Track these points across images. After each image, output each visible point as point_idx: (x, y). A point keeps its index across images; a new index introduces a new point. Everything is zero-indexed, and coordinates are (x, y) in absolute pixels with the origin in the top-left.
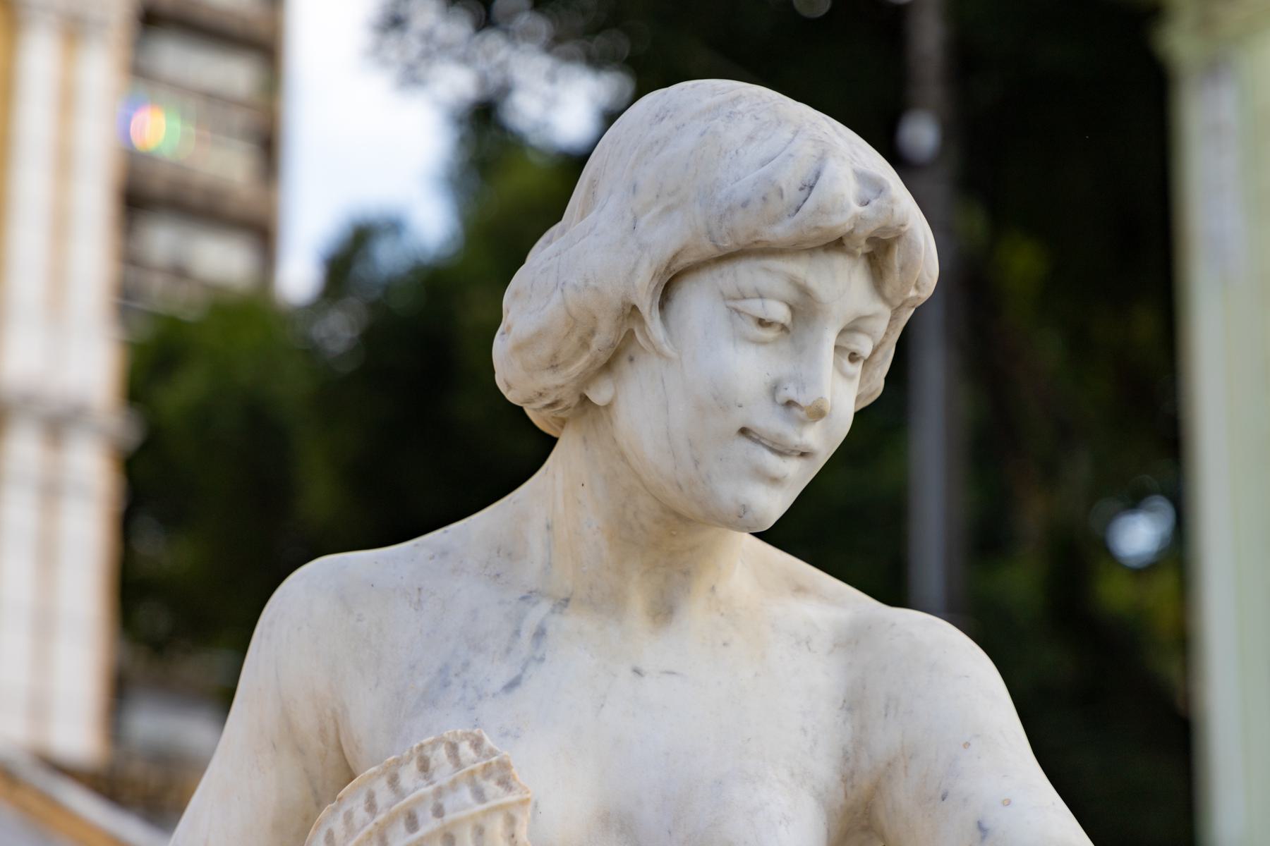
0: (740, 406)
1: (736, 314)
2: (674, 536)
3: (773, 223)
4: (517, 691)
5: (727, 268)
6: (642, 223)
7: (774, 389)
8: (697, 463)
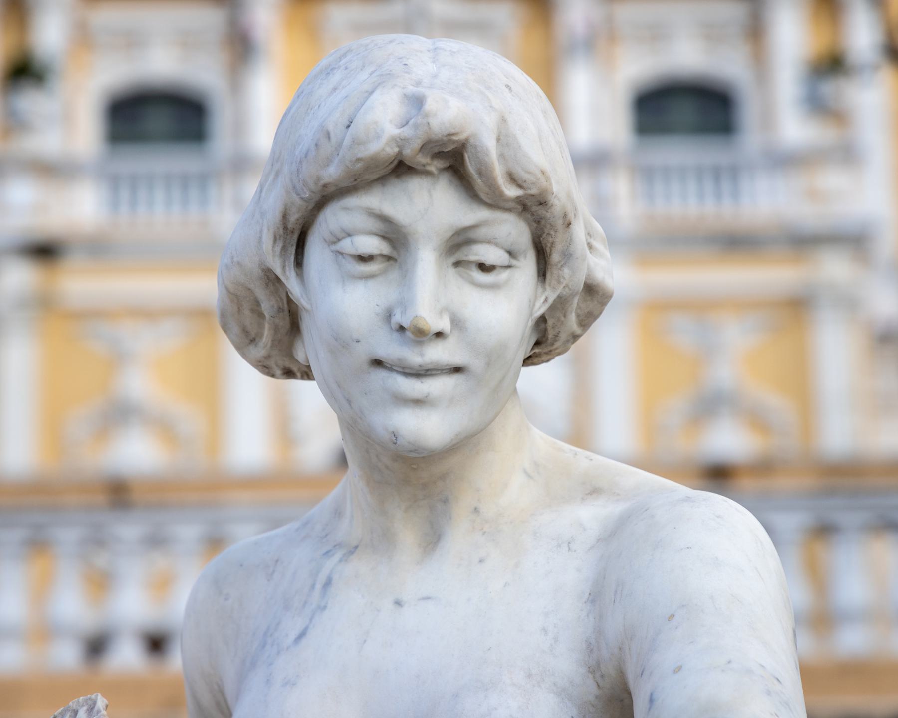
0: (358, 341)
1: (340, 257)
2: (414, 469)
3: (328, 165)
4: (304, 641)
7: (388, 315)
8: (349, 402)
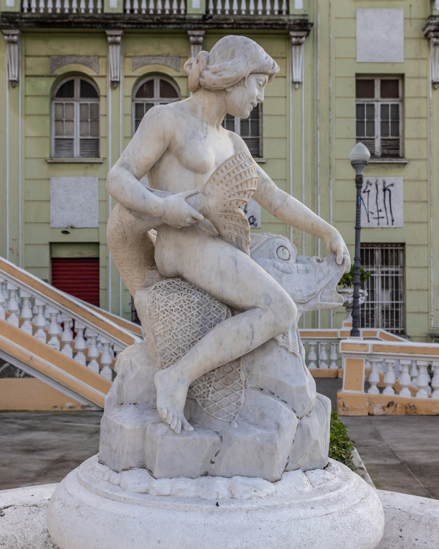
5: (259, 75)
6: (249, 63)
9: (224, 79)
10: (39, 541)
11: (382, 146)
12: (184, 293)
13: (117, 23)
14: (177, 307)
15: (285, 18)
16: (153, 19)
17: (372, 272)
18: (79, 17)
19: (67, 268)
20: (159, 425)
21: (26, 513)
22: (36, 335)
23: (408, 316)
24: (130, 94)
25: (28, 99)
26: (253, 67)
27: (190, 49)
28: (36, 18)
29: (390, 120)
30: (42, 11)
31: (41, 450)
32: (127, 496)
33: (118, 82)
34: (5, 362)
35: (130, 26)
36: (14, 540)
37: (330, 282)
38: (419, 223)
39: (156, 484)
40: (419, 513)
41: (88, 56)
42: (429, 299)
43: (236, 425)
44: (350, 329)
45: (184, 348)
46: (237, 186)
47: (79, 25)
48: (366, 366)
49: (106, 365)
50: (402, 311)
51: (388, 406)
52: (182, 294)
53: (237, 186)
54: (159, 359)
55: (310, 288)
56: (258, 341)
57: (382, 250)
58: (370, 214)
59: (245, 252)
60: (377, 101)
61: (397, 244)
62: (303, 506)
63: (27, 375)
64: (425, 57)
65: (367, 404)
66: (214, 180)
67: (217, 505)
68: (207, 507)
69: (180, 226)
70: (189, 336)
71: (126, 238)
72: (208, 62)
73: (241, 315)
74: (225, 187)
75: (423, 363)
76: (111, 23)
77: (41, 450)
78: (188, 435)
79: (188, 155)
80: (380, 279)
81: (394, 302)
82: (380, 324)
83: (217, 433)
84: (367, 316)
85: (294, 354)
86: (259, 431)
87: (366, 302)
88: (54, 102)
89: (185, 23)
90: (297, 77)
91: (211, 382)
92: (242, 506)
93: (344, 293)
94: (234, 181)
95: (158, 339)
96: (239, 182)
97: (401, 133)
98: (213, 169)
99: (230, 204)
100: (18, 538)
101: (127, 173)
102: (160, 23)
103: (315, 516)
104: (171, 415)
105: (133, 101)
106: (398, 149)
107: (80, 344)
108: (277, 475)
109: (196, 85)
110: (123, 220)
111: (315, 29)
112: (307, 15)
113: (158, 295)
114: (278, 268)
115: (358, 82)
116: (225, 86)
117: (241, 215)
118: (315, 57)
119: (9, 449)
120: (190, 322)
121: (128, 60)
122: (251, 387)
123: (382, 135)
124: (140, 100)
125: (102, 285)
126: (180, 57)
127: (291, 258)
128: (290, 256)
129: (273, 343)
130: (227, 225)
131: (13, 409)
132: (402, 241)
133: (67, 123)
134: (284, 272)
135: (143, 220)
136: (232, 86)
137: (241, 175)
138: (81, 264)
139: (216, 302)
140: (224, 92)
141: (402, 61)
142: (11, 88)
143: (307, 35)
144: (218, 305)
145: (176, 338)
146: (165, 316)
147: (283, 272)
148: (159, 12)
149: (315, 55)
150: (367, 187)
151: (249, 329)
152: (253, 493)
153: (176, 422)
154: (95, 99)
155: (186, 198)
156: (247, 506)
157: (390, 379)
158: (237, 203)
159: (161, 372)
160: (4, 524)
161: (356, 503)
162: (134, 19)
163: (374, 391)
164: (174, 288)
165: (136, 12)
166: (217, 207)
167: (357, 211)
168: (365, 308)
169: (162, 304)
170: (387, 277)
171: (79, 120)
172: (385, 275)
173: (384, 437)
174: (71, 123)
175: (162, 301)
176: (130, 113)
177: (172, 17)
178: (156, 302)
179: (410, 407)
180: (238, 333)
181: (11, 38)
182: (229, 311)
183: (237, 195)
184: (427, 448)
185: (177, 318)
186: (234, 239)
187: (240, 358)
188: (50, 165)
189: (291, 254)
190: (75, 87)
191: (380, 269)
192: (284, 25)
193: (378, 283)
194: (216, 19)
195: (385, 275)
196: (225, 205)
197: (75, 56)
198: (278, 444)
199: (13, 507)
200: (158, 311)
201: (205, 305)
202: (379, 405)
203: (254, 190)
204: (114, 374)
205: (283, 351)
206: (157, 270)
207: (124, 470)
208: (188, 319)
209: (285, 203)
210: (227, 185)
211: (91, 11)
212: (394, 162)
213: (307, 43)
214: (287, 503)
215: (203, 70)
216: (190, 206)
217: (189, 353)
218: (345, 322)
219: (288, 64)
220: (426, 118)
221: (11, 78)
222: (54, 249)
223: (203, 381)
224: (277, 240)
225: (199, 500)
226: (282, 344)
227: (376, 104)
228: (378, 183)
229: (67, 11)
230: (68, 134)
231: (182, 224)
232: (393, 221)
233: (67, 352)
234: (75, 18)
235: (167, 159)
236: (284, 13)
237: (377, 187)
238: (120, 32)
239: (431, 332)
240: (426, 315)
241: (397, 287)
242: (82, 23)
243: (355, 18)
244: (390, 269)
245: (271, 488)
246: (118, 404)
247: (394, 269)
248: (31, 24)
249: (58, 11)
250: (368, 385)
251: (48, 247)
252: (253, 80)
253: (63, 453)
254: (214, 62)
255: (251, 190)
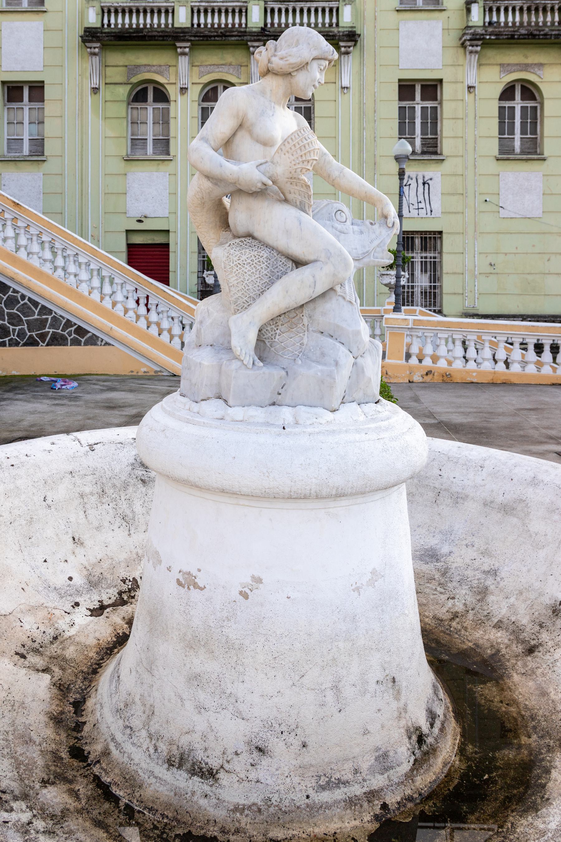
5: (320, 60)
9: (290, 64)
10: (124, 473)
11: (422, 144)
12: (254, 249)
13: (185, 36)
14: (249, 261)
15: (335, 30)
16: (217, 32)
17: (413, 258)
18: (152, 31)
19: (142, 253)
20: (233, 361)
21: (113, 449)
22: (115, 308)
23: (445, 297)
24: (197, 99)
25: (108, 104)
26: (315, 54)
27: (250, 59)
28: (115, 33)
29: (429, 121)
30: (120, 26)
31: (120, 407)
32: (206, 421)
33: (186, 89)
34: (89, 332)
35: (197, 38)
36: (103, 471)
37: (381, 242)
38: (455, 213)
39: (230, 411)
40: (457, 455)
41: (160, 66)
42: (464, 281)
43: (300, 362)
44: (392, 307)
45: (255, 297)
46: (301, 156)
47: (152, 38)
48: (407, 340)
49: (176, 335)
50: (439, 293)
51: (427, 374)
52: (253, 250)
53: (301, 156)
54: (233, 307)
55: (364, 247)
56: (320, 290)
57: (421, 238)
58: (411, 205)
59: (307, 214)
60: (418, 104)
61: (435, 233)
62: (358, 431)
63: (107, 344)
64: (461, 63)
65: (408, 372)
66: (282, 151)
67: (284, 428)
68: (275, 430)
69: (252, 191)
70: (258, 286)
71: (204, 203)
72: (275, 50)
73: (304, 267)
74: (291, 156)
75: (458, 337)
76: (180, 36)
77: (120, 407)
78: (258, 369)
79: (258, 130)
80: (420, 264)
81: (432, 284)
82: (419, 304)
83: (284, 368)
84: (408, 296)
85: (350, 302)
86: (320, 367)
87: (406, 284)
88: (130, 106)
89: (246, 36)
90: (346, 82)
91: (278, 326)
92: (305, 430)
93: (387, 275)
94: (299, 151)
95: (232, 289)
96: (303, 153)
97: (439, 132)
98: (279, 142)
99: (295, 172)
100: (106, 469)
101: (205, 145)
102: (223, 35)
103: (369, 440)
104: (244, 353)
105: (199, 105)
106: (436, 147)
107: (153, 316)
108: (335, 405)
109: (265, 70)
110: (202, 187)
111: (362, 39)
112: (355, 27)
113: (232, 251)
114: (336, 229)
115: (400, 86)
116: (291, 70)
117: (304, 181)
118: (362, 65)
119: (92, 405)
120: (260, 274)
121: (195, 69)
122: (313, 331)
123: (422, 134)
124: (205, 105)
125: (171, 268)
126: (241, 66)
127: (348, 221)
128: (346, 219)
129: (332, 293)
130: (292, 191)
131: (95, 373)
132: (441, 230)
133: (142, 125)
134: (341, 232)
135: (219, 186)
136: (296, 70)
137: (305, 146)
138: (153, 249)
139: (283, 257)
140: (289, 76)
141: (441, 67)
142: (93, 94)
143: (355, 45)
144: (284, 260)
145: (247, 288)
146: (238, 268)
147: (341, 232)
148: (223, 26)
149: (362, 62)
150: (408, 181)
151: (311, 279)
152: (315, 420)
153: (248, 358)
154: (166, 104)
155: (257, 166)
156: (309, 430)
157: (429, 350)
158: (301, 171)
159: (234, 317)
160: (95, 457)
161: (404, 431)
162: (201, 33)
163: (414, 361)
164: (246, 245)
165: (202, 26)
166: (284, 174)
167: (399, 203)
168: (406, 290)
169: (236, 259)
170: (426, 262)
171: (152, 122)
172: (424, 260)
173: (423, 401)
174: (145, 125)
175: (236, 256)
176: (197, 116)
177: (235, 30)
178: (231, 256)
179: (447, 375)
180: (302, 282)
181: (93, 50)
182: (294, 265)
183: (301, 163)
184: (462, 410)
185: (249, 271)
186: (298, 203)
187: (303, 305)
188: (126, 162)
189: (348, 217)
190: (149, 93)
191: (419, 255)
192: (334, 36)
193: (418, 267)
194: (274, 32)
195: (424, 260)
196: (291, 173)
197: (149, 65)
198: (336, 378)
199: (102, 444)
200: (232, 265)
201: (273, 260)
202: (419, 374)
203: (316, 160)
204: (183, 344)
205: (341, 299)
206: (231, 231)
207: (203, 400)
208: (258, 272)
209: (342, 174)
210: (293, 155)
211: (163, 26)
212: (432, 158)
213: (355, 52)
214: (344, 429)
215: (272, 56)
216: (260, 174)
217: (258, 301)
218: (388, 300)
219: (337, 71)
220: (463, 119)
221: (93, 86)
222: (129, 236)
223: (271, 325)
224: (335, 205)
225: (268, 424)
226: (340, 294)
227: (416, 106)
228: (418, 177)
229: (141, 26)
230: (143, 135)
231: (254, 189)
232: (431, 211)
233: (142, 324)
234: (149, 32)
235: (240, 134)
236: (334, 25)
237: (417, 181)
238: (188, 44)
239: (465, 311)
240: (461, 296)
241: (435, 271)
242: (155, 36)
243: (399, 29)
244: (428, 255)
245: (330, 416)
246: (197, 346)
247: (432, 255)
248: (110, 38)
249: (134, 26)
250: (408, 356)
251: (125, 234)
252: (315, 65)
253: (139, 410)
254: (281, 50)
255: (314, 159)
